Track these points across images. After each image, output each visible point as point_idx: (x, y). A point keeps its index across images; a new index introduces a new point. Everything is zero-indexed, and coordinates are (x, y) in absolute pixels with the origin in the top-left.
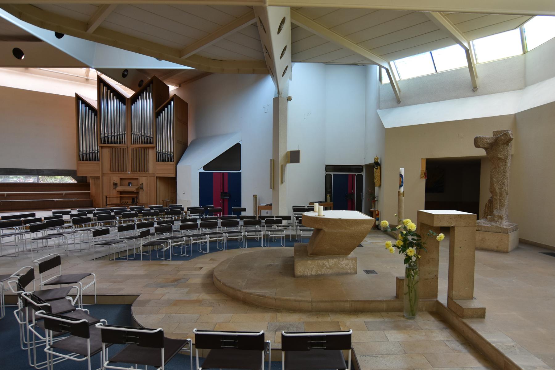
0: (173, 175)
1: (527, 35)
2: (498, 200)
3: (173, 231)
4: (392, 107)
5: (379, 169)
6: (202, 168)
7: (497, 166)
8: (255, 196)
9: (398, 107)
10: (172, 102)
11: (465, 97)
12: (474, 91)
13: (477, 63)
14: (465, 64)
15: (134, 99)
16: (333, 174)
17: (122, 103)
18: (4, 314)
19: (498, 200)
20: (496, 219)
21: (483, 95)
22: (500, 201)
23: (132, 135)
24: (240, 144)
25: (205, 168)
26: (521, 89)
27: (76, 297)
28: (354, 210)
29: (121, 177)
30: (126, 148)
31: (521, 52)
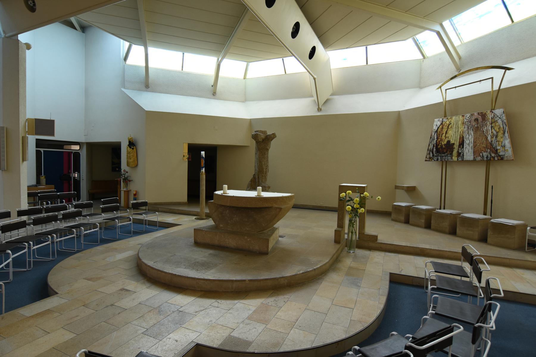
1: (249, 67)
2: (264, 176)
4: (139, 90)
5: (135, 149)
7: (264, 154)
9: (146, 91)
11: (206, 98)
12: (214, 95)
14: (144, 64)
16: (44, 151)
19: (264, 176)
20: (267, 189)
21: (220, 99)
22: (265, 177)
26: (243, 102)
28: (28, 202)
31: (243, 77)
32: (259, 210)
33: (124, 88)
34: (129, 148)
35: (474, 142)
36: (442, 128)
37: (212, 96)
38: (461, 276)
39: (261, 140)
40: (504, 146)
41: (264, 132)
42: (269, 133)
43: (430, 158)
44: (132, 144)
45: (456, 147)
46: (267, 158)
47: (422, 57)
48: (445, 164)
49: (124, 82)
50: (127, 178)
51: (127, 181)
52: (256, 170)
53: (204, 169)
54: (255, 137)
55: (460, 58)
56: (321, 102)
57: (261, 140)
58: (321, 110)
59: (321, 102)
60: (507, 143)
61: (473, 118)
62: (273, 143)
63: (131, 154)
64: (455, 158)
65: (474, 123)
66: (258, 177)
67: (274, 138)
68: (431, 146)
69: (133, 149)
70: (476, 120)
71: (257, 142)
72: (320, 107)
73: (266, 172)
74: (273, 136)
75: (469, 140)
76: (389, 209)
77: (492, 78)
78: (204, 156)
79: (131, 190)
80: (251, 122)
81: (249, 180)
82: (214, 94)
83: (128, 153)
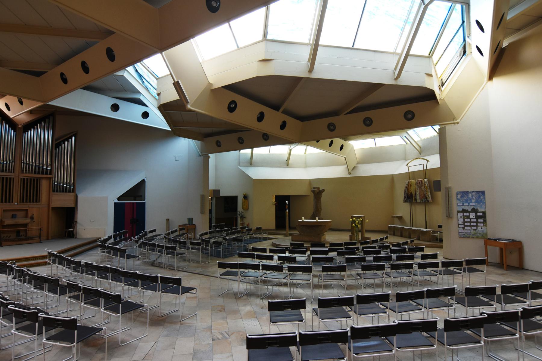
0: (73, 206)
3: (210, 244)
6: (117, 199)
8: (168, 220)
10: (74, 137)
12: (287, 165)
13: (536, 347)
15: (28, 126)
17: (11, 129)
18: (94, 327)
23: (23, 164)
24: (144, 180)
25: (119, 199)
27: (45, 330)
29: (4, 209)
30: (13, 177)
31: (304, 153)
32: (318, 226)
33: (239, 166)
34: (244, 200)
35: (420, 194)
36: (408, 186)
37: (286, 166)
38: (524, 298)
39: (316, 193)
40: (428, 196)
41: (318, 188)
42: (321, 189)
43: (405, 201)
44: (245, 197)
45: (414, 195)
46: (321, 202)
47: (405, 143)
48: (411, 204)
49: (239, 163)
50: (242, 216)
51: (242, 217)
52: (314, 209)
53: (287, 210)
54: (313, 191)
55: (420, 147)
56: (350, 169)
57: (316, 193)
58: (350, 173)
59: (350, 169)
60: (429, 194)
61: (418, 182)
62: (323, 194)
63: (245, 203)
64: (414, 201)
65: (419, 185)
66: (316, 213)
67: (324, 191)
68: (405, 195)
69: (246, 200)
70: (419, 183)
71: (315, 194)
72: (350, 172)
73: (320, 211)
74: (324, 190)
75: (418, 193)
76: (386, 229)
77: (423, 164)
78: (287, 203)
79: (244, 223)
80: (310, 181)
81: (311, 215)
82: (288, 165)
83: (243, 202)
